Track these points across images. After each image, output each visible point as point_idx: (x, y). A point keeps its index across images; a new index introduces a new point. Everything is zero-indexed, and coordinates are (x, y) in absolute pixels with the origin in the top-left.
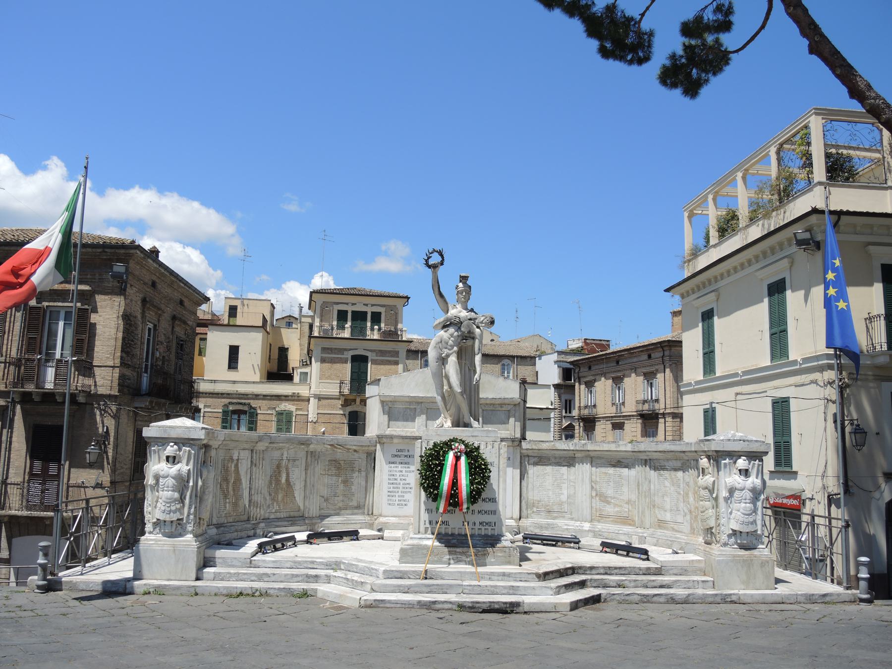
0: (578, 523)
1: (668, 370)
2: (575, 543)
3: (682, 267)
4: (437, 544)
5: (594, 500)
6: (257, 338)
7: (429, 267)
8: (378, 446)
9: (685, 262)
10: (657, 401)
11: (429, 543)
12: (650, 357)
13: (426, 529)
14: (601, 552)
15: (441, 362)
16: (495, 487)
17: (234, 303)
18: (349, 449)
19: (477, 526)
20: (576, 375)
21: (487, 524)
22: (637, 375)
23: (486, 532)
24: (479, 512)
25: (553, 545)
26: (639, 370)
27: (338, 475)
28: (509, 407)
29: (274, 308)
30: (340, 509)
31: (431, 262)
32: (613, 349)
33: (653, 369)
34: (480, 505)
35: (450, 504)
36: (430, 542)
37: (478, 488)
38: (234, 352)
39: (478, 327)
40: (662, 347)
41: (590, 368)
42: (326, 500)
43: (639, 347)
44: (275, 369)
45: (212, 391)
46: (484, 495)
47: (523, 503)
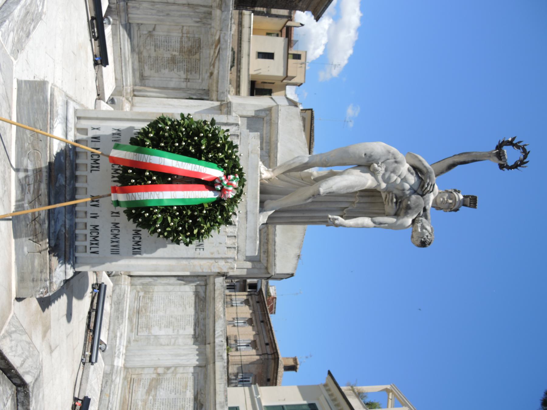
0: (123, 350)
1: (258, 357)
2: (91, 357)
3: (348, 385)
4: (57, 147)
5: (151, 371)
6: (280, 73)
7: (499, 147)
8: (217, 104)
9: (352, 387)
10: (237, 350)
11: (58, 131)
12: (267, 344)
13: (84, 131)
14: (76, 399)
15: (363, 162)
16: (160, 252)
17: (303, 57)
18: (214, 65)
19: (91, 222)
20: (253, 293)
21: (95, 238)
22: (254, 336)
23: (80, 238)
24: (116, 225)
25: (88, 325)
26: (257, 336)
27: (181, 51)
28: (264, 262)
29: (299, 86)
30: (140, 53)
31: (506, 150)
32: (270, 315)
33: (259, 347)
34: (128, 227)
35: (125, 169)
36: (60, 136)
37: (155, 222)
38: (270, 56)
39: (414, 221)
40: (274, 353)
41: (258, 302)
42: (150, 34)
43: (273, 337)
44: (258, 86)
45: (243, 39)
46: (145, 232)
47: (150, 280)
